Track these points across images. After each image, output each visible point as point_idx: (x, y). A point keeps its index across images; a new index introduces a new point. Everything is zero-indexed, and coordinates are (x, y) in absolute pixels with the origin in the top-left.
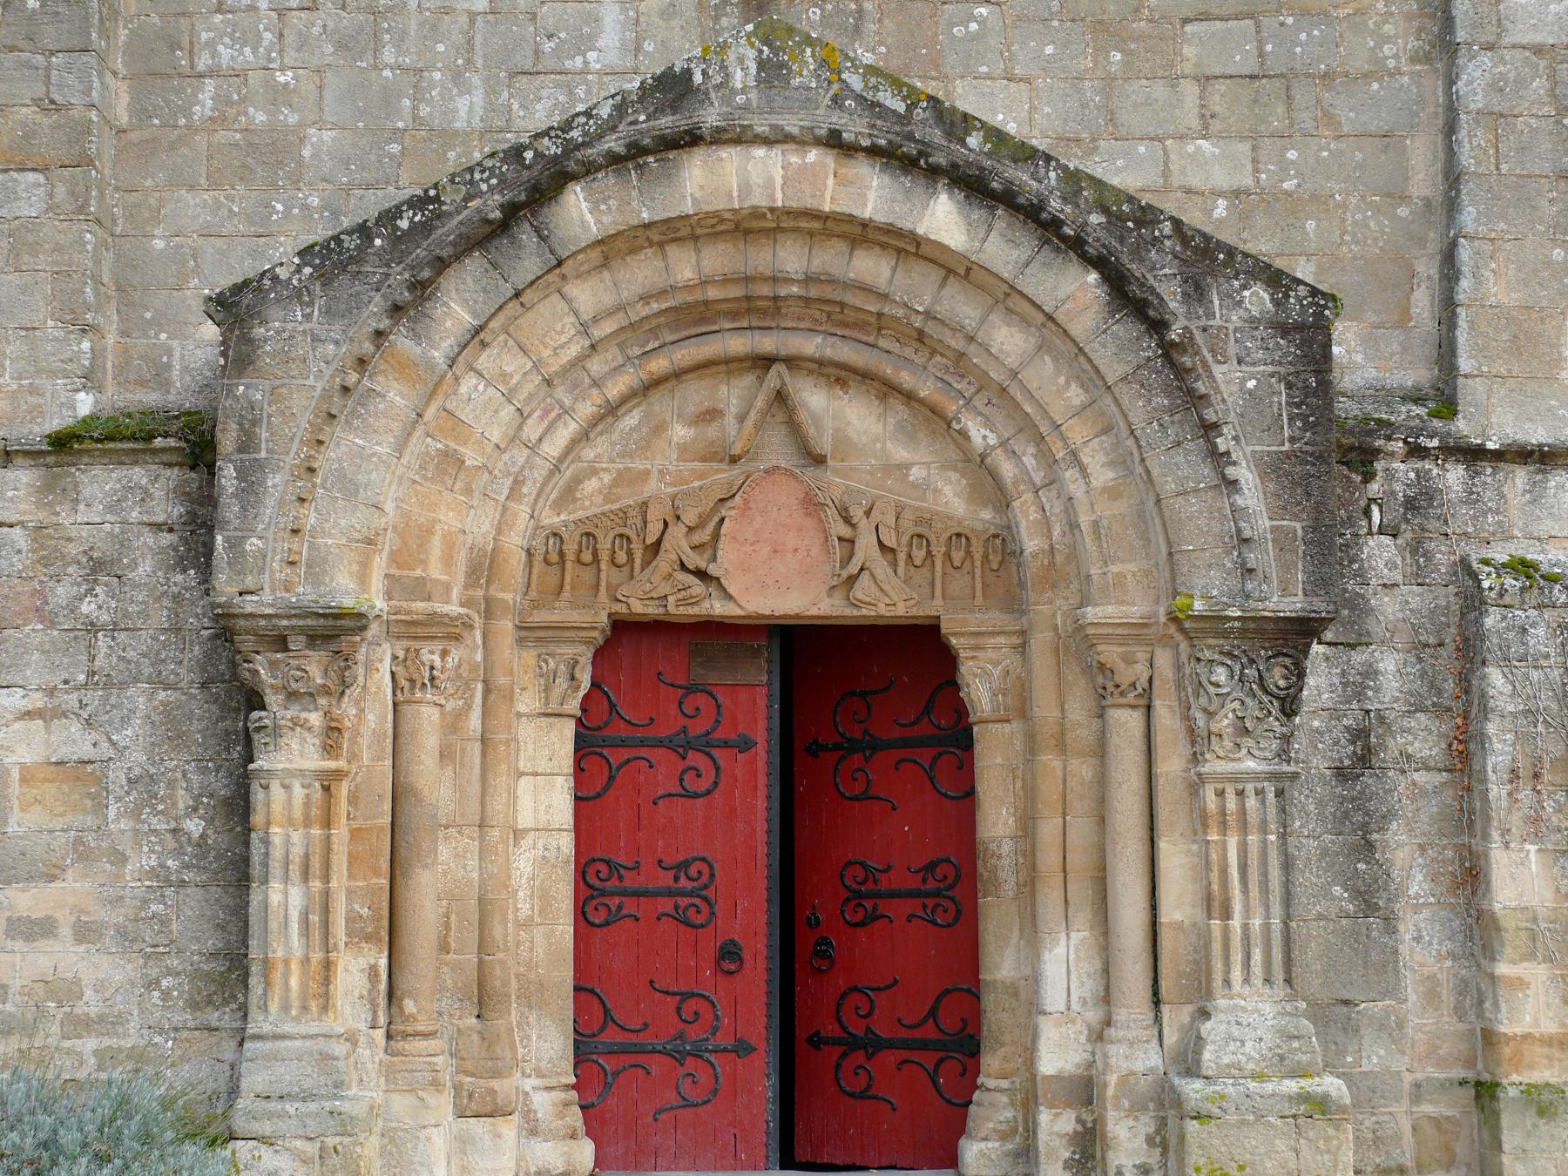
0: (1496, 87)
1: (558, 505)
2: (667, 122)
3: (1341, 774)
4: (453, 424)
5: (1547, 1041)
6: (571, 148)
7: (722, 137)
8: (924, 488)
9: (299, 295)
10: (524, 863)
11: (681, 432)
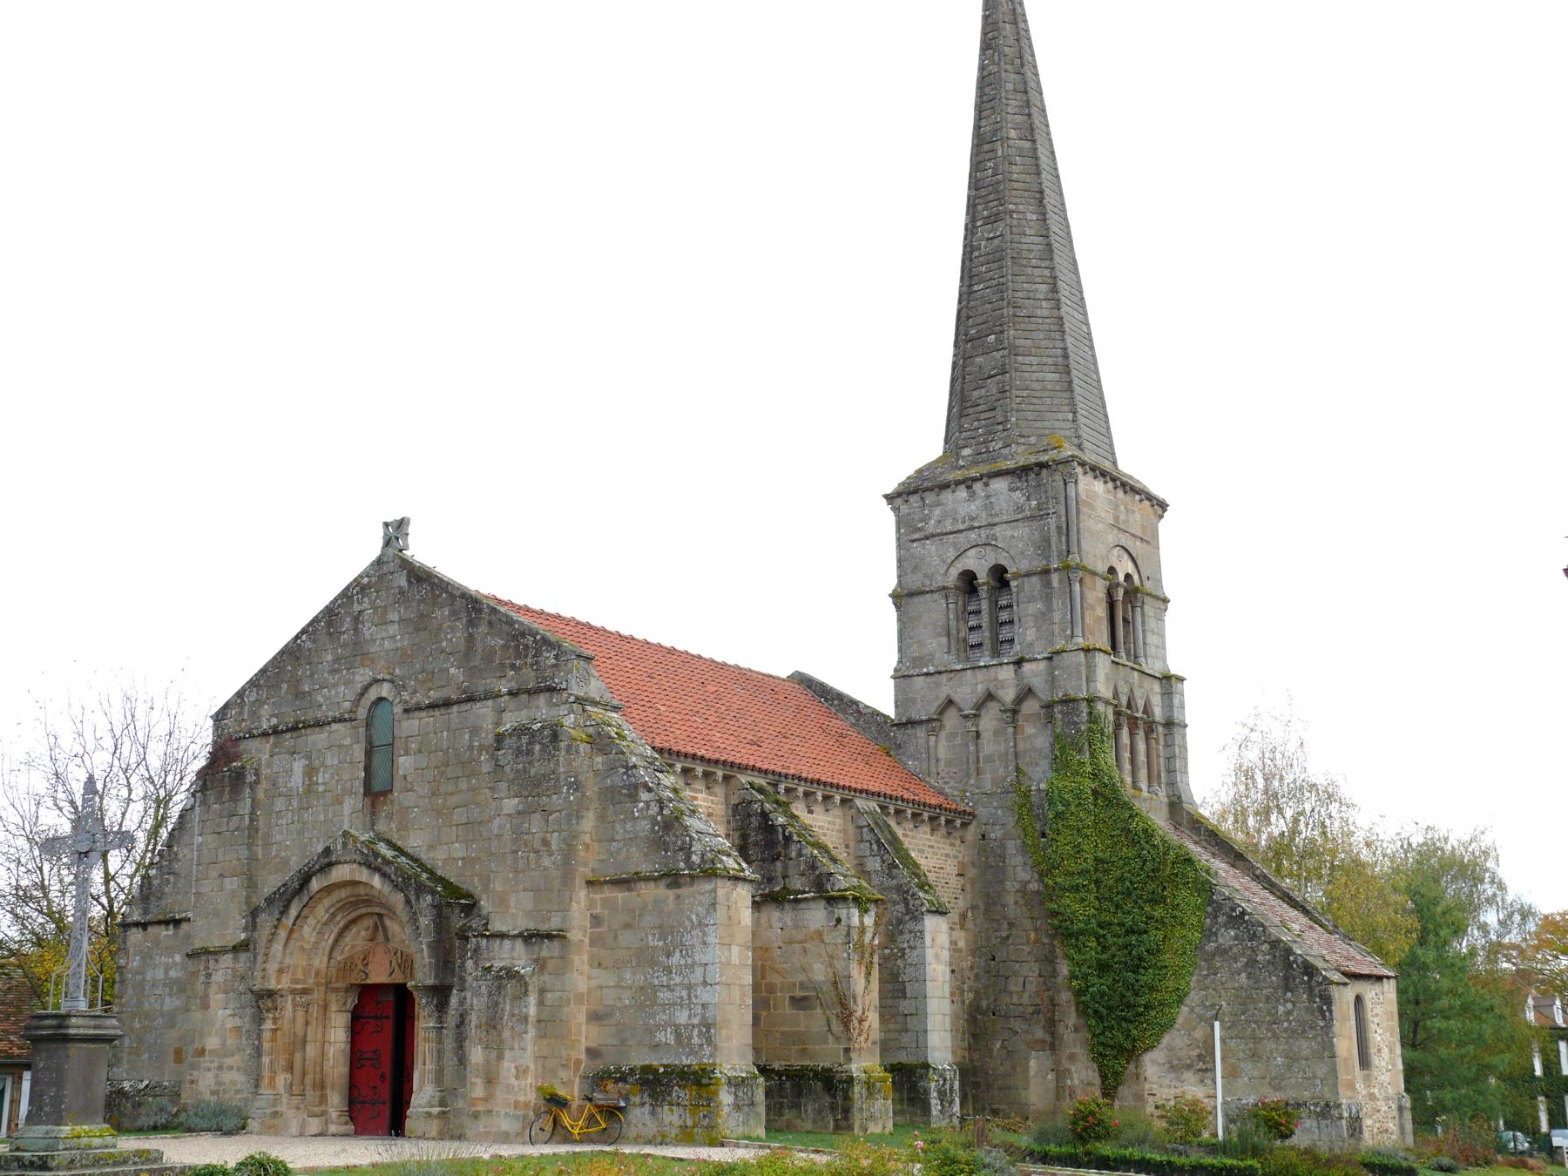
0: (500, 827)
1: (341, 955)
3: (458, 1026)
5: (481, 1099)
6: (310, 868)
7: (338, 863)
10: (331, 1051)
11: (363, 933)
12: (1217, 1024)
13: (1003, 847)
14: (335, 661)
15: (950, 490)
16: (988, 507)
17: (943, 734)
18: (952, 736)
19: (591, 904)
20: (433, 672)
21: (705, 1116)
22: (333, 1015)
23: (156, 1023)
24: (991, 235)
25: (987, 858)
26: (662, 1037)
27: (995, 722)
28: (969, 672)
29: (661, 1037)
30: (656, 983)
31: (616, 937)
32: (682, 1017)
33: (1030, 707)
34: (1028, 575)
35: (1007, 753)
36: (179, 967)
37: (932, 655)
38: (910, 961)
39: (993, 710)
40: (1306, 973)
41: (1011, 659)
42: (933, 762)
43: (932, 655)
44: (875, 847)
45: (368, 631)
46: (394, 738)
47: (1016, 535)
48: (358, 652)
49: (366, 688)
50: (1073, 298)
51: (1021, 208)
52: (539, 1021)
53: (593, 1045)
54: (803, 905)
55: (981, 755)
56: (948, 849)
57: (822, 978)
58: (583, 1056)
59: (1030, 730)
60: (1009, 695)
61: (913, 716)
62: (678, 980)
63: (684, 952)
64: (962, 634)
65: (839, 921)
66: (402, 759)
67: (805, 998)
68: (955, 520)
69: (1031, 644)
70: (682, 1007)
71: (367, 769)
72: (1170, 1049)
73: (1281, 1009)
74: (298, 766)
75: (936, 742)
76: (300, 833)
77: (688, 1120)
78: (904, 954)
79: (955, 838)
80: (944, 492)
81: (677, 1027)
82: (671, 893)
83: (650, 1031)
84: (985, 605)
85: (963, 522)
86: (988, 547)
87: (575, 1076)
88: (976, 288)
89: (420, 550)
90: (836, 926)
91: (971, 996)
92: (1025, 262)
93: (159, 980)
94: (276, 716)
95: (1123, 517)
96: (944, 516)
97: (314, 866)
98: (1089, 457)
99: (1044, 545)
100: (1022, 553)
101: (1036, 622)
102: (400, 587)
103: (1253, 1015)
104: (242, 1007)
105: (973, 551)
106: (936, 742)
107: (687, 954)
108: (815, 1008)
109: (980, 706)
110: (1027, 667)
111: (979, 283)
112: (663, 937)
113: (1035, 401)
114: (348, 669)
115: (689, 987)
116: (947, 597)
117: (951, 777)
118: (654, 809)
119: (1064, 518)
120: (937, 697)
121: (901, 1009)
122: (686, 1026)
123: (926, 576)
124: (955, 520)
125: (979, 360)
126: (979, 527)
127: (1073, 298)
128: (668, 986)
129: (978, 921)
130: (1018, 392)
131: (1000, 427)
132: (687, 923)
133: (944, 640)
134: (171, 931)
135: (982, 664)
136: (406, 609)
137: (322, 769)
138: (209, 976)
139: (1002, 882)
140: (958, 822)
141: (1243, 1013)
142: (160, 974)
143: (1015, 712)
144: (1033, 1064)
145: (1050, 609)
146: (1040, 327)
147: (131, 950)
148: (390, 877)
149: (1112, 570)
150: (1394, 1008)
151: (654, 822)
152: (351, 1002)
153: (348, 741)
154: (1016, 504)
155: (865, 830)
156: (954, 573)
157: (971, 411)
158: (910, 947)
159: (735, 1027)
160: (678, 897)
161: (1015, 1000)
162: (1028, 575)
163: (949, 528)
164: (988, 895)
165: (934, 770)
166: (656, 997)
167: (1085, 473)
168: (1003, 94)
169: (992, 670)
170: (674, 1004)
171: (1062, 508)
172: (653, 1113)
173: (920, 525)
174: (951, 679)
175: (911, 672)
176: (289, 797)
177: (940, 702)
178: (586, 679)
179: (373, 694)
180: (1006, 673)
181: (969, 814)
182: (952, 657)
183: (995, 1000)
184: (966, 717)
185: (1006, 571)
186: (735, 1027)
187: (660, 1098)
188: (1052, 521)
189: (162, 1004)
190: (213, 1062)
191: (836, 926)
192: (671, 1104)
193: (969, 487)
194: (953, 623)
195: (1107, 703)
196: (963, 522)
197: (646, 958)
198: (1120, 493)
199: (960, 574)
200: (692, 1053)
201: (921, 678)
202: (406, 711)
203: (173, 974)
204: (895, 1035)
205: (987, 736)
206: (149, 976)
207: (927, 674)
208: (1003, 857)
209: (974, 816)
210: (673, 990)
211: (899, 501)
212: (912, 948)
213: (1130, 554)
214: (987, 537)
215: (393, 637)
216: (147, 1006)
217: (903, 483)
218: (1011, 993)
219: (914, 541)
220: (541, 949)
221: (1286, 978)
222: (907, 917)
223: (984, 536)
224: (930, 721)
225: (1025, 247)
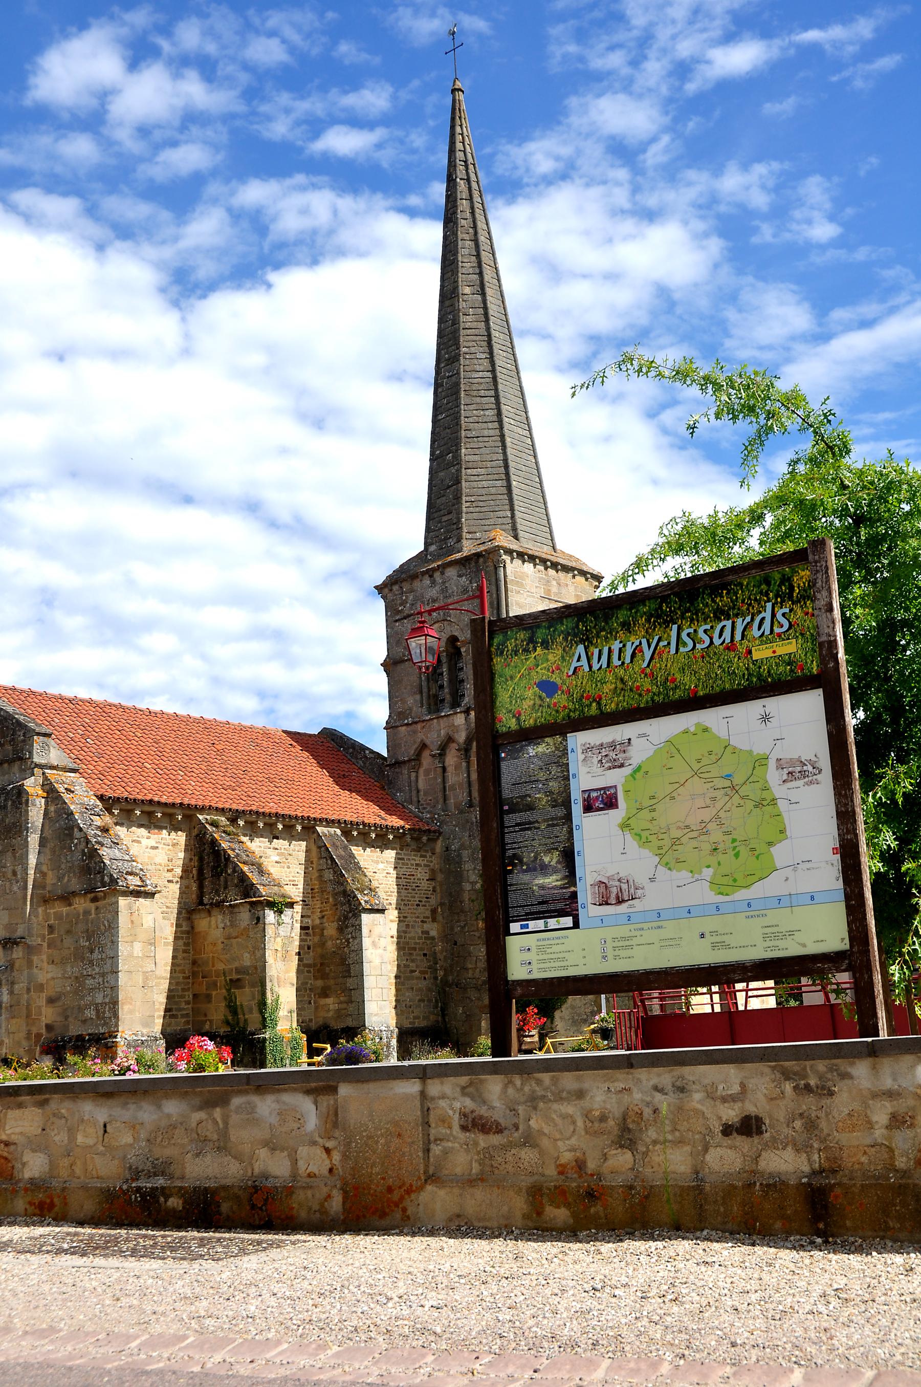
13: (459, 856)
16: (444, 590)
18: (427, 772)
19: (47, 917)
26: (90, 1013)
27: (455, 759)
28: (435, 721)
31: (62, 941)
32: (99, 999)
37: (411, 709)
38: (353, 948)
41: (462, 709)
43: (411, 709)
44: (329, 862)
50: (517, 418)
53: (49, 1022)
54: (236, 910)
55: (447, 785)
56: (418, 860)
57: (249, 964)
58: (44, 1031)
62: (97, 970)
64: (433, 691)
65: (258, 919)
67: (238, 980)
68: (423, 602)
72: (573, 1007)
78: (349, 943)
79: (427, 851)
83: (81, 1009)
85: (428, 604)
87: (36, 1046)
88: (440, 417)
90: (256, 924)
91: (442, 973)
92: (475, 393)
95: (554, 589)
96: (416, 599)
98: (527, 544)
106: (417, 777)
108: (244, 987)
111: (442, 413)
112: (88, 939)
113: (481, 504)
115: (103, 975)
117: (428, 804)
119: (495, 595)
120: (415, 742)
121: (348, 985)
127: (517, 418)
129: (445, 914)
130: (467, 498)
131: (455, 526)
132: (102, 927)
133: (418, 697)
135: (443, 714)
139: (460, 884)
140: (425, 838)
146: (486, 444)
150: (366, 966)
151: (84, 854)
154: (462, 586)
155: (323, 849)
158: (352, 937)
159: (138, 1003)
160: (97, 908)
161: (470, 975)
164: (450, 895)
165: (415, 799)
166: (85, 983)
167: (512, 559)
168: (460, 259)
169: (451, 718)
175: (398, 724)
177: (416, 746)
178: (45, 747)
181: (435, 832)
183: (458, 976)
186: (138, 1003)
191: (256, 924)
193: (431, 576)
194: (424, 684)
196: (428, 604)
197: (79, 956)
198: (551, 572)
200: (105, 1024)
201: (404, 728)
204: (344, 1006)
205: (450, 770)
207: (407, 725)
208: (459, 863)
209: (440, 833)
211: (386, 590)
212: (354, 938)
217: (389, 576)
218: (467, 969)
219: (396, 621)
222: (350, 915)
224: (410, 761)
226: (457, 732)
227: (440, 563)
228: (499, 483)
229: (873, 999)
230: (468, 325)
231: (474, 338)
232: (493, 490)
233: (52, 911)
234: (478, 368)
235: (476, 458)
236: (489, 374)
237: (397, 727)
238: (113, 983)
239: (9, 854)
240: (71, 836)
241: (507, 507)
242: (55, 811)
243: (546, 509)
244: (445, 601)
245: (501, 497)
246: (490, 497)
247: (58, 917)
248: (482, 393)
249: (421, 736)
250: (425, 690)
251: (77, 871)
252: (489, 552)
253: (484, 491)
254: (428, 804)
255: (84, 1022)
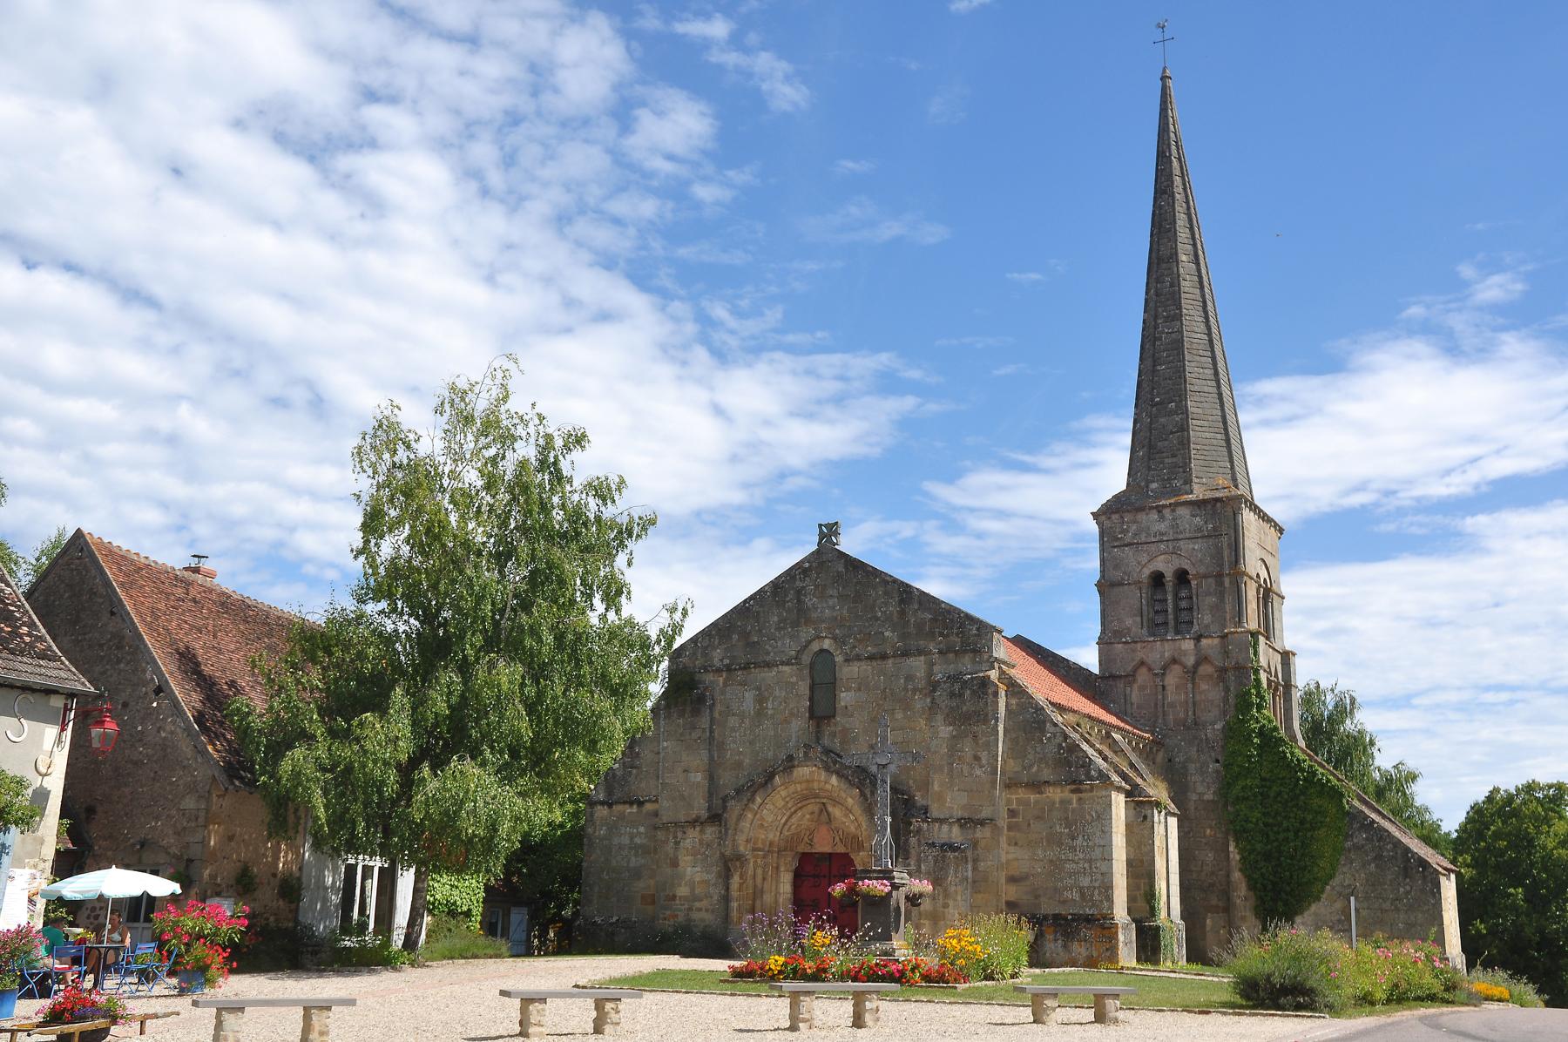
0: (936, 746)
1: (788, 831)
2: (790, 764)
4: (762, 819)
8: (848, 827)
9: (733, 798)
12: (1352, 898)
13: (1185, 767)
14: (780, 622)
15: (1144, 513)
16: (1175, 526)
17: (1135, 686)
18: (1142, 688)
19: (1009, 801)
20: (870, 634)
21: (1107, 950)
22: (782, 875)
23: (623, 875)
24: (1170, 331)
25: (1173, 775)
28: (1158, 643)
29: (1068, 895)
30: (1063, 857)
32: (1085, 882)
33: (1205, 669)
34: (1205, 576)
35: (1187, 702)
36: (643, 836)
37: (1129, 629)
39: (1176, 670)
40: (1420, 866)
42: (1129, 706)
43: (1129, 629)
45: (809, 601)
46: (835, 679)
47: (1196, 548)
48: (802, 615)
49: (809, 642)
51: (1191, 312)
52: (974, 882)
55: (1166, 702)
59: (1204, 686)
60: (1190, 661)
61: (1114, 672)
62: (1081, 856)
63: (1086, 837)
65: (1145, 817)
66: (843, 695)
68: (1148, 535)
69: (1207, 626)
70: (1085, 875)
71: (811, 699)
73: (1402, 890)
74: (749, 696)
75: (1131, 691)
76: (751, 743)
77: (1094, 952)
80: (1139, 513)
81: (1081, 889)
82: (1074, 797)
84: (1170, 597)
86: (1173, 555)
89: (848, 544)
92: (1195, 352)
93: (625, 845)
94: (728, 657)
97: (778, 768)
99: (1218, 555)
100: (1201, 561)
101: (1211, 611)
102: (838, 572)
103: (1380, 894)
104: (291, 875)
105: (1162, 557)
106: (1131, 691)
107: (1088, 838)
109: (1165, 668)
110: (1204, 642)
112: (1068, 826)
113: (1205, 453)
114: (792, 628)
116: (1141, 589)
118: (1059, 739)
120: (1133, 660)
122: (1088, 888)
123: (1124, 573)
124: (1148, 535)
125: (1162, 420)
126: (1167, 541)
128: (1073, 861)
131: (1181, 470)
133: (1138, 619)
134: (635, 809)
136: (843, 588)
137: (771, 699)
138: (677, 843)
141: (1372, 892)
142: (626, 840)
143: (1194, 673)
144: (1208, 922)
145: (1222, 600)
147: (598, 823)
148: (847, 778)
149: (1258, 575)
152: (795, 864)
153: (794, 679)
156: (1147, 572)
157: (1157, 456)
160: (1080, 799)
162: (1205, 576)
163: (1143, 540)
165: (1129, 711)
169: (1178, 643)
170: (1079, 872)
171: (1232, 531)
172: (1065, 946)
173: (1120, 536)
174: (1144, 647)
176: (742, 716)
177: (1134, 663)
179: (815, 647)
180: (1188, 645)
182: (1145, 631)
184: (1156, 674)
185: (1188, 574)
187: (1071, 937)
188: (1225, 540)
189: (628, 862)
190: (684, 905)
192: (1078, 941)
193: (1159, 512)
194: (1145, 608)
195: (1265, 671)
199: (1152, 573)
201: (1120, 645)
202: (847, 660)
203: (638, 841)
205: (1170, 689)
206: (616, 841)
210: (1078, 863)
213: (1266, 565)
214: (1174, 548)
215: (833, 608)
216: (614, 863)
219: (1115, 547)
220: (975, 832)
221: (1405, 869)
223: (1171, 547)
225: (1195, 341)
226: (1185, 655)
227: (1172, 501)
228: (1219, 436)
229: (353, 901)
230: (1186, 290)
231: (1192, 302)
232: (1215, 442)
233: (1014, 797)
234: (1196, 329)
235: (1200, 411)
236: (1205, 337)
237: (1114, 643)
238: (1104, 869)
239: (970, 739)
240: (1043, 731)
241: (1227, 459)
242: (1017, 704)
243: (1246, 465)
244: (1175, 535)
245: (1220, 449)
246: (1213, 448)
247: (1027, 803)
248: (1201, 353)
249: (1140, 655)
250: (1145, 613)
251: (1050, 762)
252: (1229, 499)
253: (1207, 442)
254: (1142, 717)
255: (1064, 902)
